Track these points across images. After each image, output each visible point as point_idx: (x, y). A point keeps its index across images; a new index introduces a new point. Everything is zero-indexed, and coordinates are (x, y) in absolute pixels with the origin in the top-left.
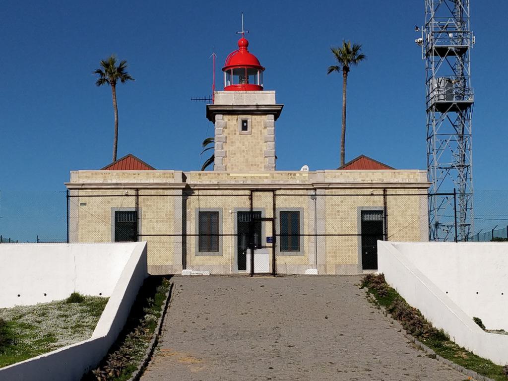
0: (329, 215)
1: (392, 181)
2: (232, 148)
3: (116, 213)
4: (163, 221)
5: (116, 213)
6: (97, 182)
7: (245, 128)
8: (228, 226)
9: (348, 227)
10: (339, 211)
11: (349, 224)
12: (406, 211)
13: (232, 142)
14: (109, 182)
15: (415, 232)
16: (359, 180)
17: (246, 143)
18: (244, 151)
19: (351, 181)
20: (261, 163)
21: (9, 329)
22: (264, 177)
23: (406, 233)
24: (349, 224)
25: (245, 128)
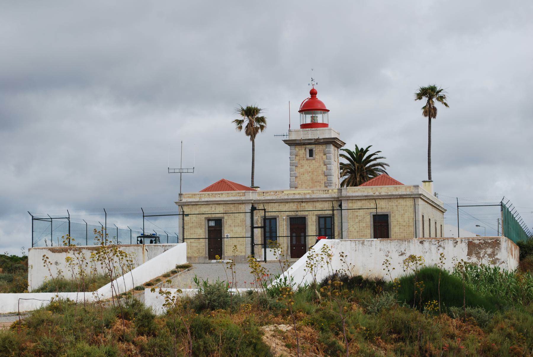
0: (350, 218)
1: (394, 193)
2: (302, 170)
3: (387, 215)
4: (238, 226)
5: (387, 215)
6: (195, 200)
7: (311, 155)
8: (283, 229)
9: (364, 227)
10: (357, 216)
11: (364, 225)
12: (404, 214)
13: (302, 166)
14: (203, 200)
15: (410, 229)
16: (371, 193)
17: (312, 166)
18: (310, 172)
19: (366, 194)
20: (322, 180)
21: (318, 335)
22: (307, 193)
23: (404, 230)
24: (364, 225)
25: (311, 155)
